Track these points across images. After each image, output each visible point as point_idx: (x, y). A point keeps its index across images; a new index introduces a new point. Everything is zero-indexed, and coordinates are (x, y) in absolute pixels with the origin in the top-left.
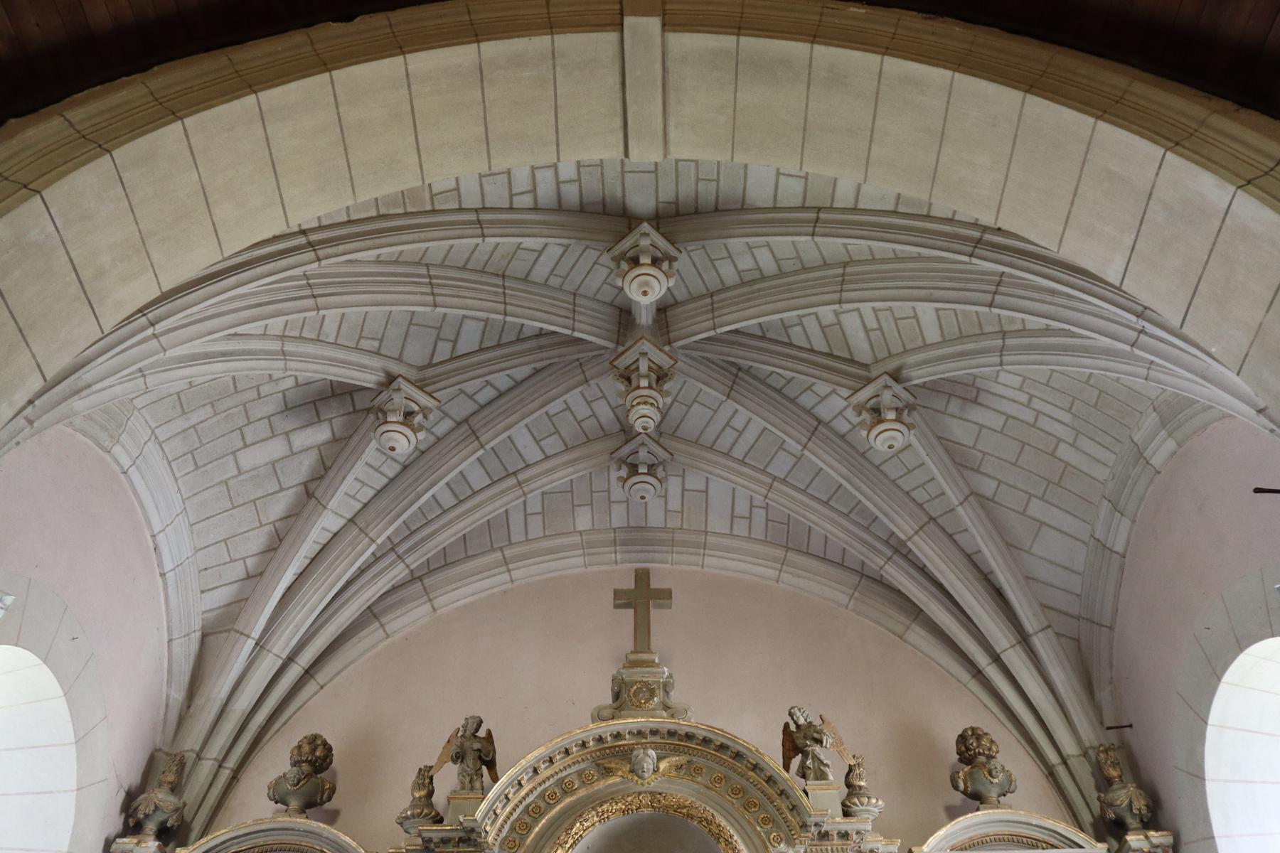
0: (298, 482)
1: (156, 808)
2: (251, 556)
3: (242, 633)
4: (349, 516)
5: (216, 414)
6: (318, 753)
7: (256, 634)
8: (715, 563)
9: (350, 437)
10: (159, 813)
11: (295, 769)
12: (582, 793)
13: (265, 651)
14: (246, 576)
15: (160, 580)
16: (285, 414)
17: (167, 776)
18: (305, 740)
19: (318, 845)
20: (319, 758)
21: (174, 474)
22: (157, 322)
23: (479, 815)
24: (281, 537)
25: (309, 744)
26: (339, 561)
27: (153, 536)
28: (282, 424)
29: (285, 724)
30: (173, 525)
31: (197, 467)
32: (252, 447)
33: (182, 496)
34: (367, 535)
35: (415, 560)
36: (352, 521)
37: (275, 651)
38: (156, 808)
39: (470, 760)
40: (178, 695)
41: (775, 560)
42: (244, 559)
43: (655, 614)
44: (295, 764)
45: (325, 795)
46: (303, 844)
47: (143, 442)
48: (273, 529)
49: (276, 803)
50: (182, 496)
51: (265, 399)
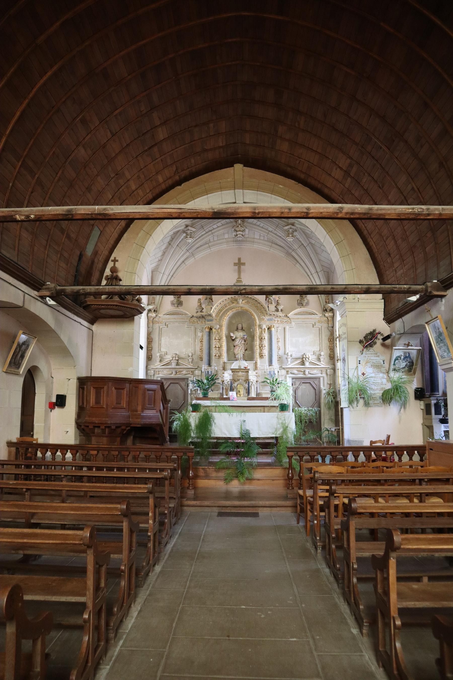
8: (256, 246)
12: (229, 307)
23: (211, 312)
39: (208, 299)
41: (269, 246)
43: (242, 267)
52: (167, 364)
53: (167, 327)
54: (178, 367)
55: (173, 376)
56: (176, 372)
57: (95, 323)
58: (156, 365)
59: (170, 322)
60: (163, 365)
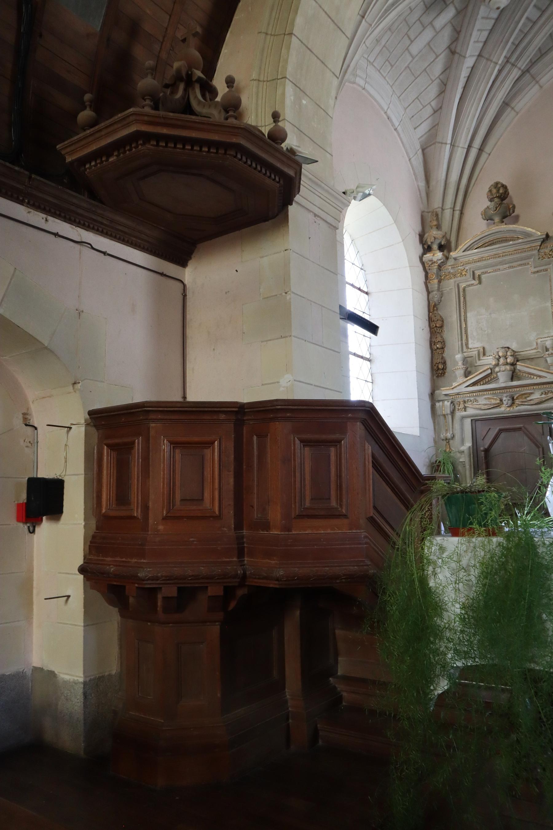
0: (444, 49)
1: (435, 238)
2: (433, 100)
3: (442, 143)
4: (477, 54)
5: (392, 33)
6: (501, 191)
7: (449, 141)
9: (466, 7)
10: (436, 240)
11: (493, 203)
13: (456, 147)
14: (434, 112)
15: (395, 133)
16: (427, 12)
17: (433, 223)
18: (492, 187)
19: (516, 235)
20: (502, 193)
21: (382, 75)
22: (365, 14)
24: (445, 83)
25: (495, 188)
26: (480, 83)
27: (386, 113)
28: (426, 19)
29: (476, 180)
30: (391, 102)
31: (392, 66)
32: (415, 41)
33: (390, 85)
34: (491, 61)
35: (523, 64)
36: (480, 55)
37: (461, 145)
38: (435, 238)
40: (422, 184)
42: (429, 103)
44: (491, 200)
45: (511, 211)
46: (508, 236)
47: (365, 68)
48: (439, 81)
49: (487, 220)
50: (390, 85)
51: (414, 10)
52: (489, 378)
53: (480, 283)
54: (515, 383)
55: (503, 409)
56: (513, 399)
57: (191, 258)
58: (455, 384)
59: (486, 267)
60: (474, 384)
